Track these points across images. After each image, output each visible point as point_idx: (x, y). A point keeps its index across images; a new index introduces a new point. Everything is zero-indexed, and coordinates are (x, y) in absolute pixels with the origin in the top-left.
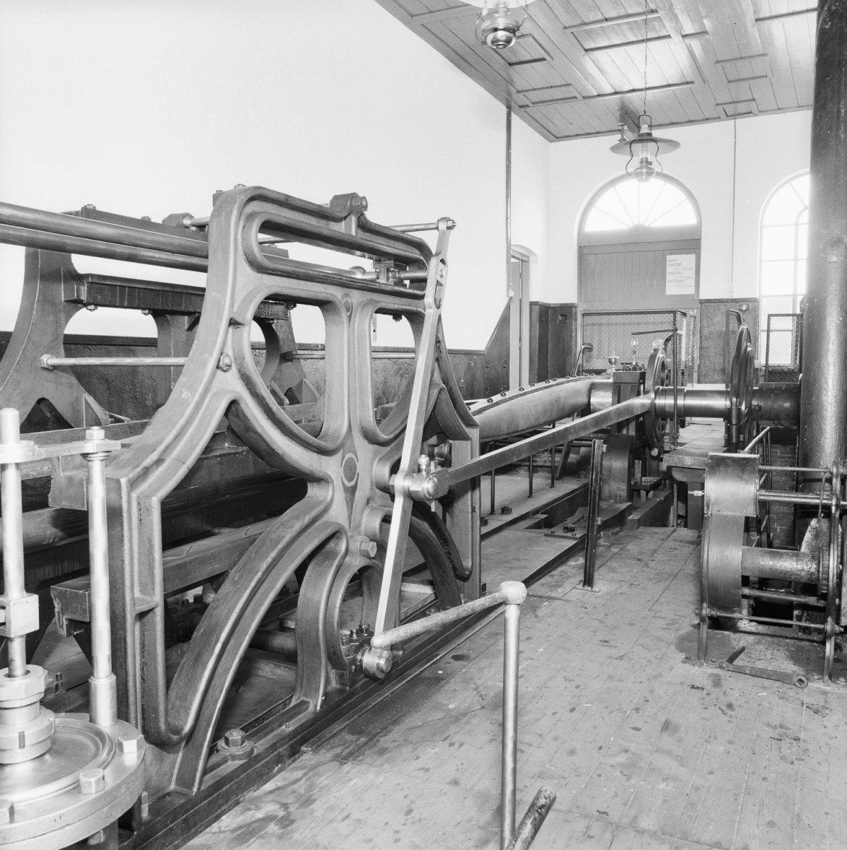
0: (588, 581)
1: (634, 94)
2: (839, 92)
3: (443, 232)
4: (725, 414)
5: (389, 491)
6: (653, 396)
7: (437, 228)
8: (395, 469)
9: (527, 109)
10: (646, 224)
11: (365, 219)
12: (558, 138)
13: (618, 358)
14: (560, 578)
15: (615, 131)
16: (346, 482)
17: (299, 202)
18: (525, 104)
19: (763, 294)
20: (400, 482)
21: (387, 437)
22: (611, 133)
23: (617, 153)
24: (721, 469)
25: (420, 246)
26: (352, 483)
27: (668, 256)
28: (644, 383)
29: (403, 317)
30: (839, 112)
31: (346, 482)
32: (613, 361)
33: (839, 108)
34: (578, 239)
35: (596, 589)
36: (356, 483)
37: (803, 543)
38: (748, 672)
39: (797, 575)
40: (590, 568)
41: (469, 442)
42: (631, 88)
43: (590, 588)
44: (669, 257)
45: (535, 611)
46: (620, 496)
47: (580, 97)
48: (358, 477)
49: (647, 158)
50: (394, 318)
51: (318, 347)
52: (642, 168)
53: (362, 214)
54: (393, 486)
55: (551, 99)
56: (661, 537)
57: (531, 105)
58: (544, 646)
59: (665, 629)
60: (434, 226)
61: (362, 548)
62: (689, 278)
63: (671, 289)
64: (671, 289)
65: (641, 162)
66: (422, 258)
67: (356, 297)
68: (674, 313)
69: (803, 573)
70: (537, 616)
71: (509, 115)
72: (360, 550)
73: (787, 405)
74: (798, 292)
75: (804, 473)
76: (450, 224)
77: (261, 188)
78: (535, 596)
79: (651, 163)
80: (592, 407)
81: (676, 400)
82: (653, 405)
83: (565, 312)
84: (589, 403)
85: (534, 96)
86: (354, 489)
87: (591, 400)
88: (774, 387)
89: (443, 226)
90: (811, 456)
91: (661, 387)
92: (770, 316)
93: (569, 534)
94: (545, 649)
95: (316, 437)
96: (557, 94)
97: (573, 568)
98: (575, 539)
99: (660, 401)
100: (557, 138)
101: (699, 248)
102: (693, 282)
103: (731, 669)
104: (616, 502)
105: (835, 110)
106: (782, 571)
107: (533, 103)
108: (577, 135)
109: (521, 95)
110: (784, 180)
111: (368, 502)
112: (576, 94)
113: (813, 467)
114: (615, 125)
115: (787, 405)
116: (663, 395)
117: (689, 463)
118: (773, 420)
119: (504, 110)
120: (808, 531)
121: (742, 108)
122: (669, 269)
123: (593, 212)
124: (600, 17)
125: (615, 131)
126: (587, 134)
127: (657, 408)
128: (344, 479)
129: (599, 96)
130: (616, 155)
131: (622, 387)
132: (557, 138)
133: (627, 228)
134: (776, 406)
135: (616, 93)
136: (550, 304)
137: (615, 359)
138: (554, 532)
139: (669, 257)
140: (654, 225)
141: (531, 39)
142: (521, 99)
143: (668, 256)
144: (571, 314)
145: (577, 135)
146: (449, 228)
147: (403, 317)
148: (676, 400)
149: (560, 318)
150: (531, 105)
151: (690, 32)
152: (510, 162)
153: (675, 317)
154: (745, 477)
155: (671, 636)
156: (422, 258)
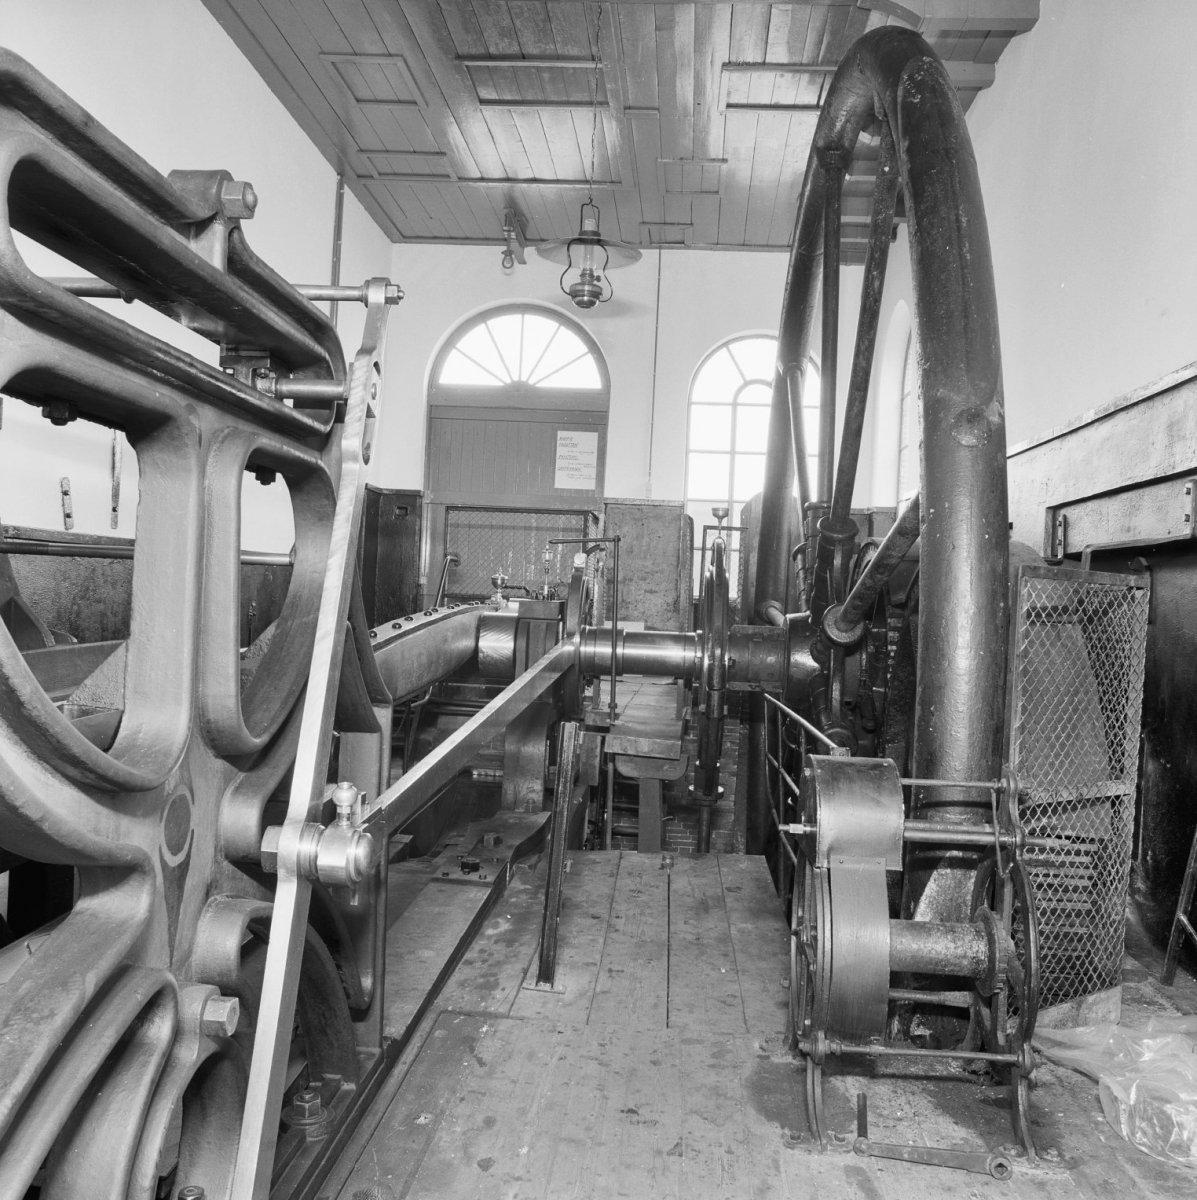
0: (546, 974)
1: (534, 185)
2: (954, 193)
3: (378, 306)
4: (686, 674)
5: (258, 872)
6: (577, 639)
7: (364, 300)
8: (274, 812)
9: (369, 182)
10: (531, 382)
11: (242, 241)
12: (406, 238)
13: (506, 578)
14: (485, 966)
15: (497, 239)
16: (168, 856)
17: (114, 144)
18: (367, 174)
19: (689, 496)
20: (289, 844)
21: (257, 741)
22: (486, 242)
23: (544, 257)
24: (841, 785)
25: (321, 329)
26: (181, 857)
27: (559, 432)
28: (563, 619)
29: (279, 476)
30: (958, 220)
31: (168, 856)
32: (499, 582)
33: (957, 215)
34: (429, 395)
35: (559, 985)
36: (188, 856)
37: (923, 898)
38: (906, 1156)
39: (955, 965)
40: (549, 951)
41: (376, 736)
42: (531, 176)
43: (547, 987)
44: (561, 434)
45: (472, 1050)
46: (534, 802)
47: (454, 177)
48: (192, 839)
49: (591, 270)
50: (257, 478)
51: (7, 531)
52: (583, 284)
53: (238, 228)
54: (274, 856)
55: (410, 172)
56: (609, 869)
57: (376, 175)
58: (527, 1138)
59: (713, 1066)
60: (356, 293)
61: (209, 1017)
62: (587, 466)
63: (563, 481)
64: (563, 481)
65: (583, 275)
66: (327, 357)
67: (206, 419)
68: (585, 513)
69: (965, 962)
70: (481, 1063)
71: (340, 186)
72: (202, 1022)
73: (771, 659)
74: (736, 497)
75: (927, 788)
76: (393, 292)
77: (18, 59)
78: (460, 1013)
79: (598, 279)
80: (481, 655)
81: (614, 647)
82: (577, 653)
83: (407, 501)
84: (476, 649)
85: (383, 163)
86: (184, 867)
87: (481, 644)
88: (750, 632)
89: (377, 296)
90: (941, 757)
91: (588, 627)
92: (706, 528)
93: (474, 877)
94: (532, 1147)
95: (106, 750)
96: (420, 165)
97: (496, 942)
98: (486, 885)
99: (588, 649)
100: (404, 237)
101: (606, 425)
102: (593, 472)
103: (876, 1153)
104: (527, 811)
105: (953, 218)
106: (931, 959)
107: (380, 174)
108: (435, 238)
109: (364, 156)
110: (719, 343)
111: (207, 895)
112: (449, 171)
113: (944, 779)
114: (494, 228)
115: (771, 659)
116: (590, 639)
117: (646, 750)
118: (749, 682)
119: (334, 177)
120: (932, 879)
121: (673, 233)
122: (560, 451)
123: (453, 357)
124: (514, 49)
125: (497, 239)
126: (451, 238)
127: (582, 659)
128: (165, 849)
129: (482, 179)
130: (540, 258)
131: (532, 624)
132: (404, 237)
133: (501, 384)
134: (757, 661)
135: (508, 180)
136: (381, 489)
137: (503, 580)
138: (447, 874)
139: (561, 434)
140: (545, 384)
141: (401, 64)
142: (362, 163)
143: (559, 432)
144: (414, 507)
145: (435, 238)
146: (390, 301)
147: (279, 476)
148: (614, 647)
149: (397, 511)
150: (376, 175)
151: (750, 60)
152: (339, 259)
153: (586, 520)
154: (883, 800)
155: (735, 1085)
156: (327, 357)
